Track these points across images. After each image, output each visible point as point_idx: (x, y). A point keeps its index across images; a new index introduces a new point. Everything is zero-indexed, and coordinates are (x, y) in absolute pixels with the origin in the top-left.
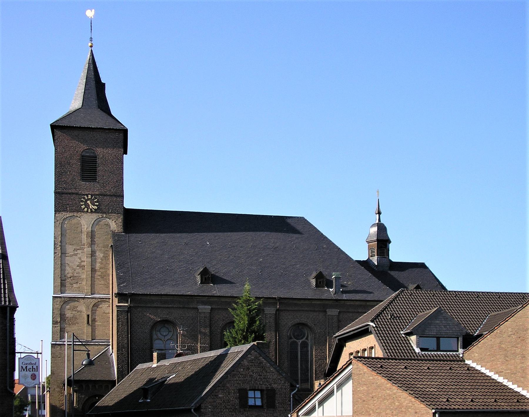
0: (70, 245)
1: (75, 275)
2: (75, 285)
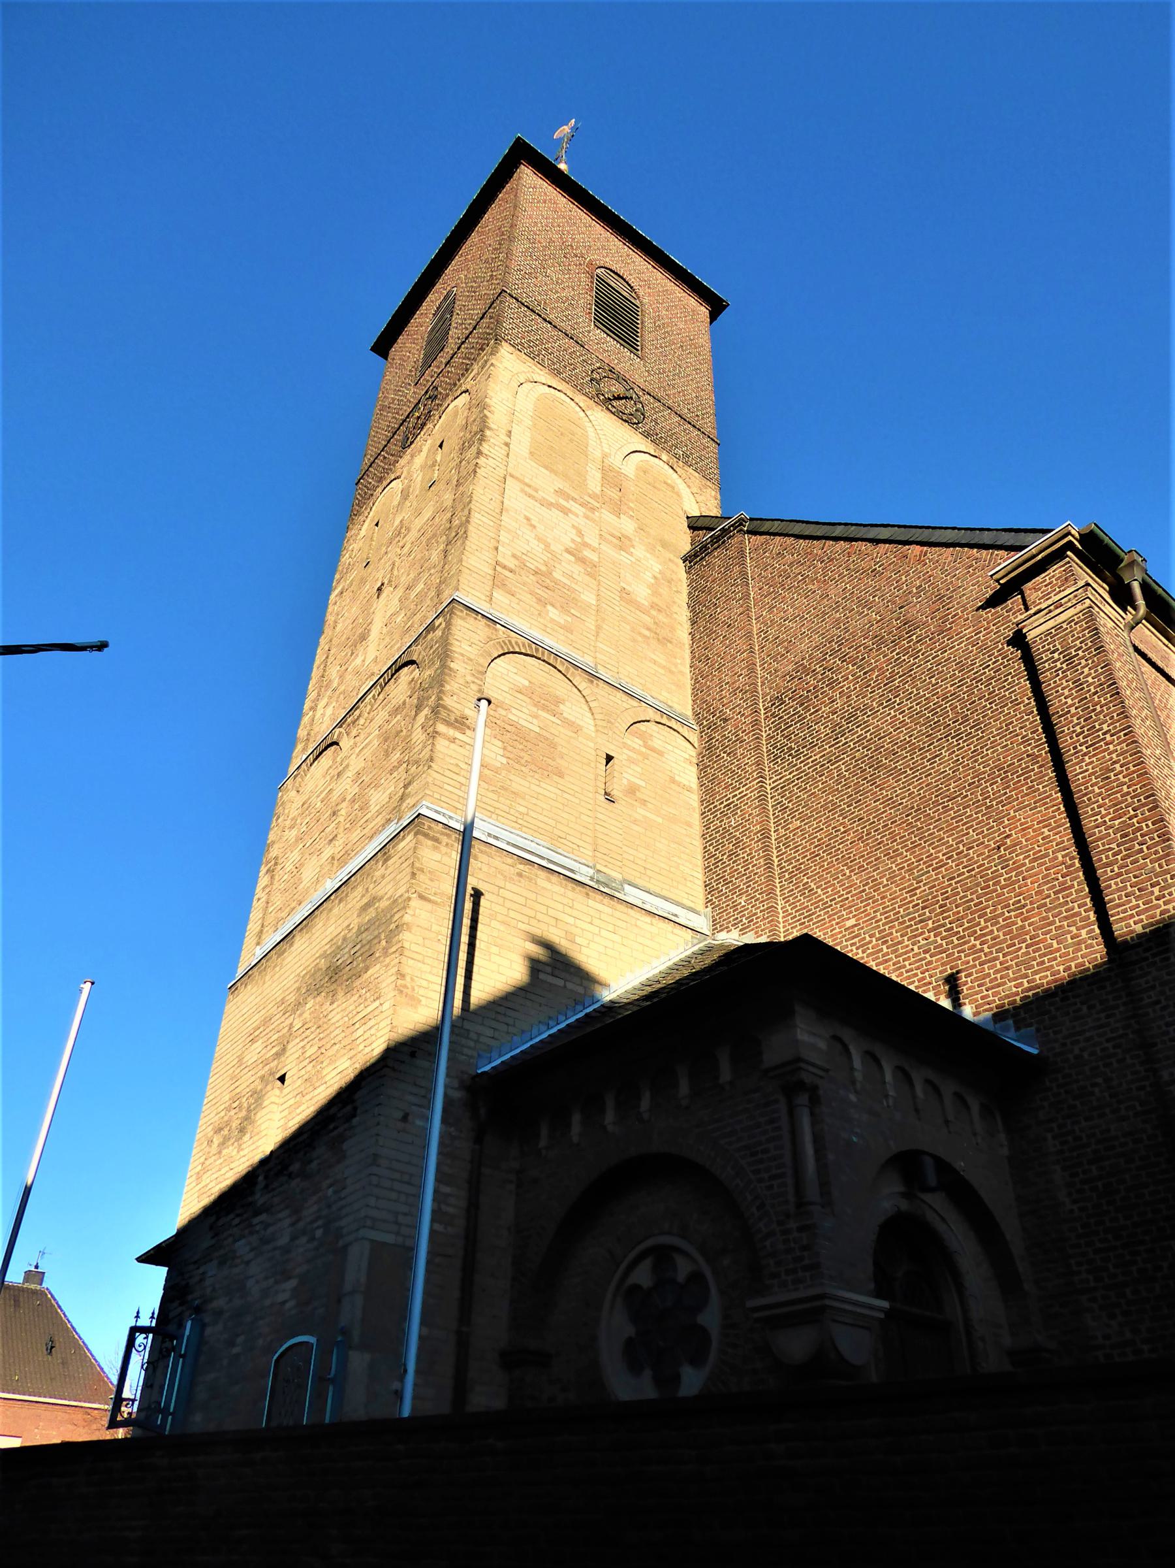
0: (546, 467)
1: (557, 575)
2: (553, 613)
